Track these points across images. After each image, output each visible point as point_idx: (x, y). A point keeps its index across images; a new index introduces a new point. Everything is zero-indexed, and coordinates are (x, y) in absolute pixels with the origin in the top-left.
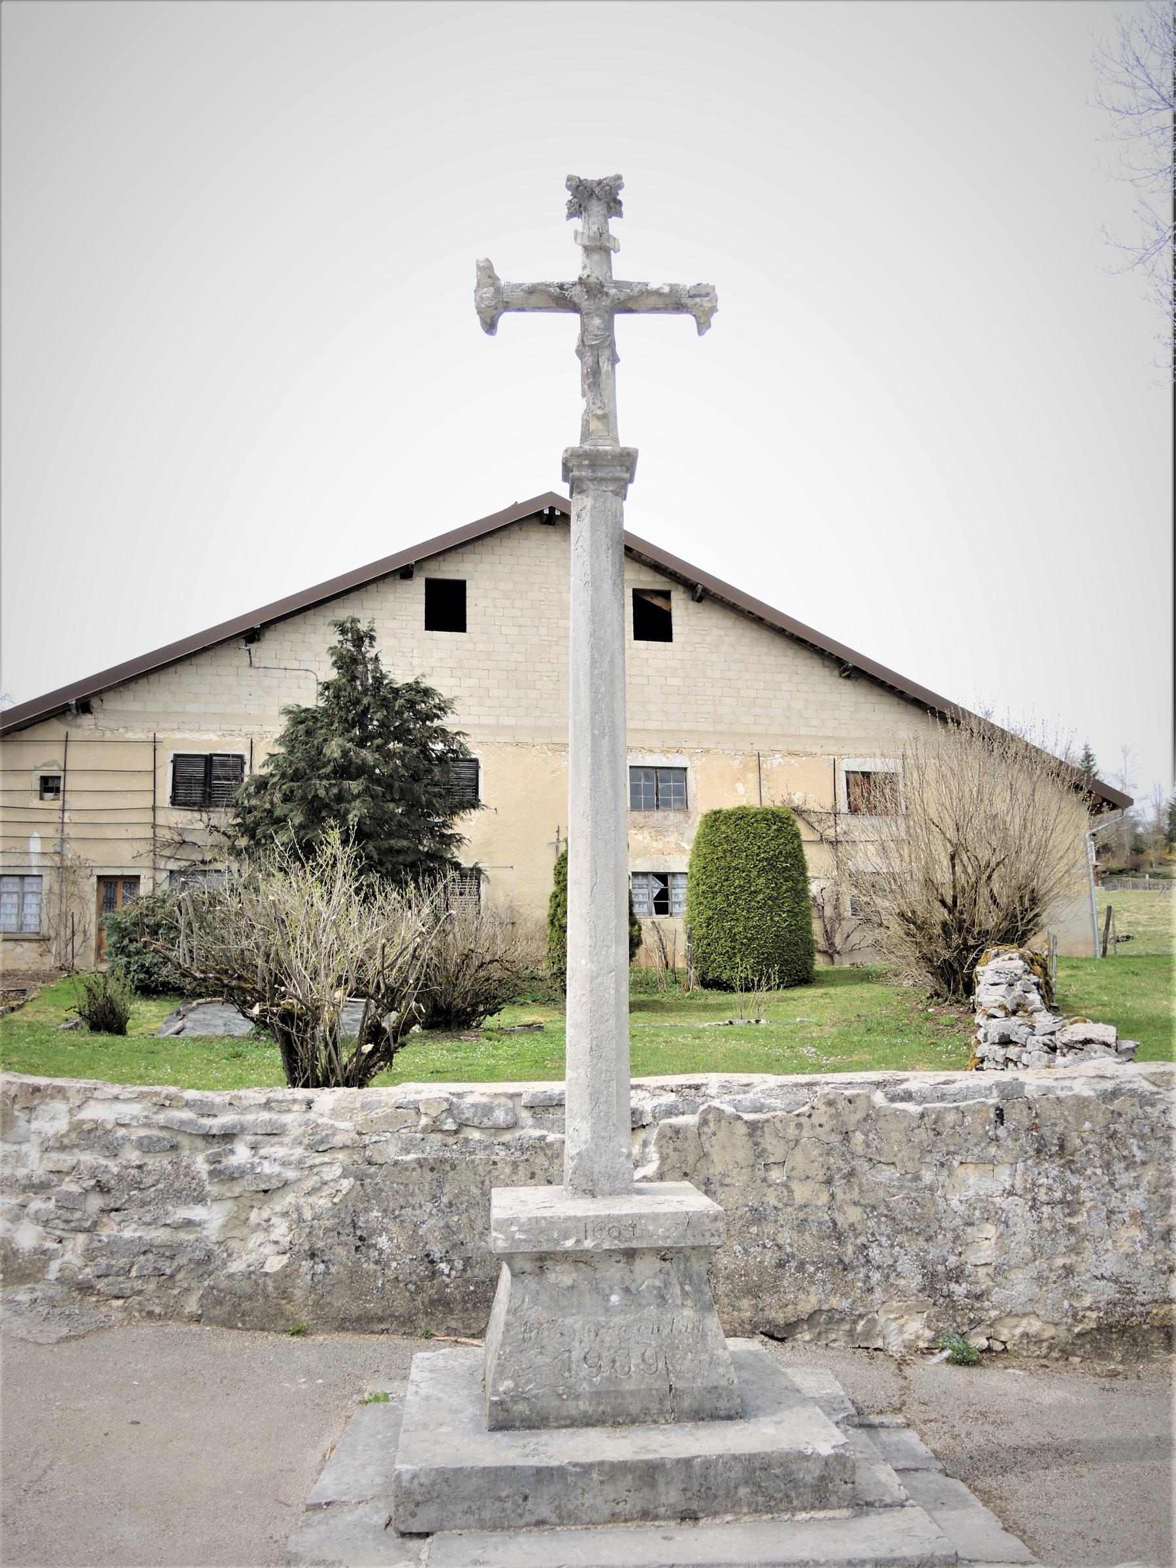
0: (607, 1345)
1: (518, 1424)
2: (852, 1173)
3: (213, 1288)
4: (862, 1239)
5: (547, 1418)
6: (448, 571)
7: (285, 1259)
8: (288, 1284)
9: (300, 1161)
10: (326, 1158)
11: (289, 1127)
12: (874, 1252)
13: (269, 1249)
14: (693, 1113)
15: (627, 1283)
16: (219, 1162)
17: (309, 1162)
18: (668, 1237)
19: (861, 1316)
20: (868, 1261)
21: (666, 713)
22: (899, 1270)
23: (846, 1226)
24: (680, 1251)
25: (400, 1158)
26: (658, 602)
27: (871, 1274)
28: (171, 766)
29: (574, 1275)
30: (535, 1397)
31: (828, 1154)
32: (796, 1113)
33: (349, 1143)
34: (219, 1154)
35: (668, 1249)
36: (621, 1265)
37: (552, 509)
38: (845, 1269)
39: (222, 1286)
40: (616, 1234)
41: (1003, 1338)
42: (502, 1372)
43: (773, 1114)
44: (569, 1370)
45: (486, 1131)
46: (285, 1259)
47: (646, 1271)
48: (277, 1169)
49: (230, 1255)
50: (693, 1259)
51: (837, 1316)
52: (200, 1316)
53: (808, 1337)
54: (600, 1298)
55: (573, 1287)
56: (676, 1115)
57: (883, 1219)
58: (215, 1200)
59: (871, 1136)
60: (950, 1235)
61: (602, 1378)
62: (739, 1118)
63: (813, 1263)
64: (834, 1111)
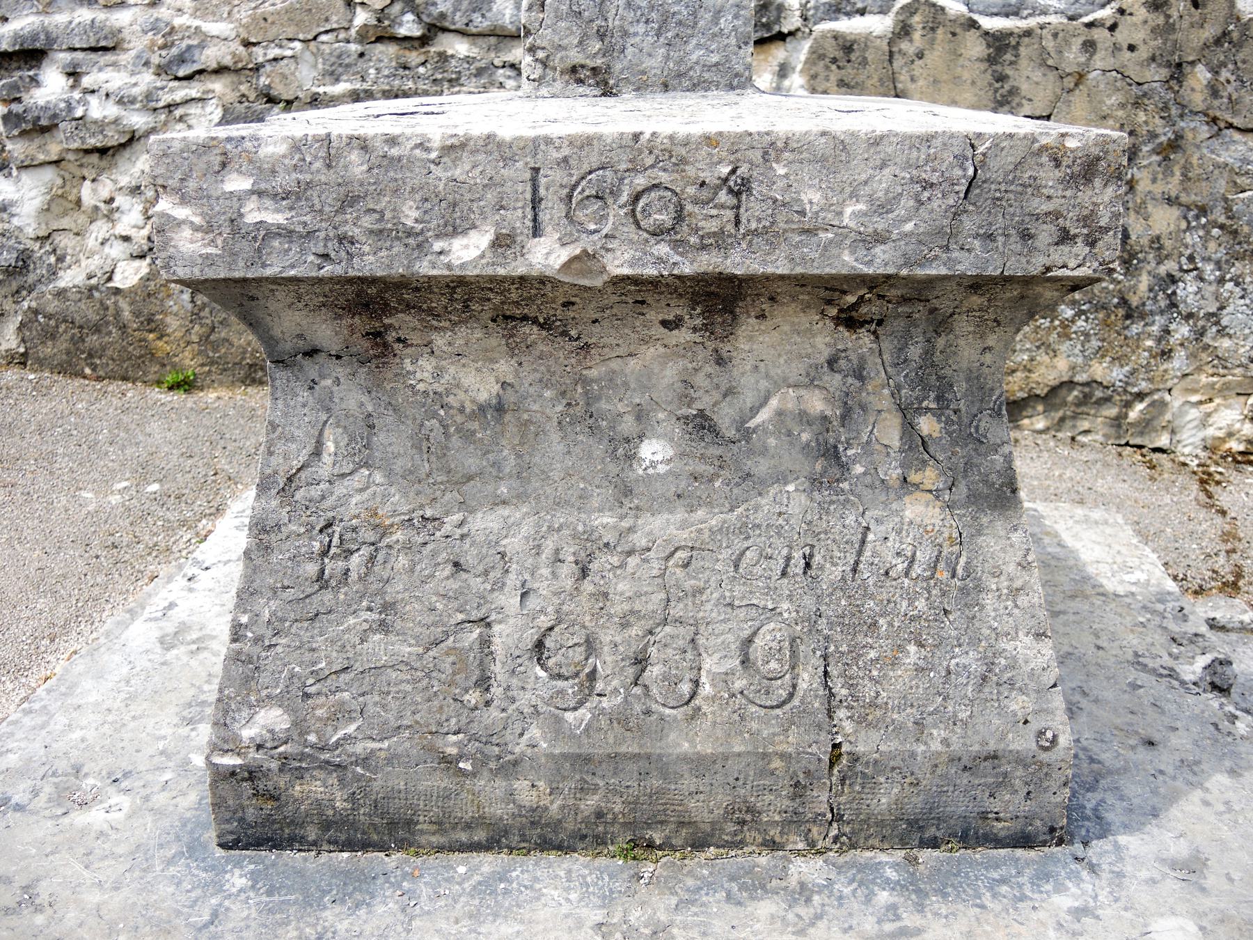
0: (618, 608)
1: (312, 833)
2: (1175, 144)
3: (36, 312)
4: (1170, 266)
5: (410, 823)
7: (143, 267)
8: (155, 309)
9: (149, 96)
10: (193, 90)
11: (126, 34)
12: (1187, 290)
13: (116, 250)
14: (883, 11)
15: (704, 402)
16: (18, 100)
17: (166, 98)
18: (880, 238)
19: (1140, 396)
20: (1173, 305)
22: (1224, 322)
23: (1145, 241)
24: (918, 292)
25: (321, 90)
27: (1172, 327)
29: (505, 367)
30: (365, 761)
31: (1136, 105)
32: (1086, 20)
33: (228, 61)
34: (15, 87)
35: (872, 283)
36: (683, 336)
38: (1128, 316)
39: (51, 309)
40: (664, 218)
42: (247, 680)
43: (1042, 19)
44: (484, 683)
45: (480, 41)
46: (143, 267)
47: (776, 367)
48: (112, 110)
49: (60, 259)
50: (963, 325)
51: (1099, 394)
52: (25, 355)
53: (1040, 425)
54: (599, 449)
55: (500, 408)
56: (848, 14)
57: (1216, 232)
58: (23, 167)
59: (1225, 74)
61: (598, 713)
62: (973, 24)
64: (1161, 20)
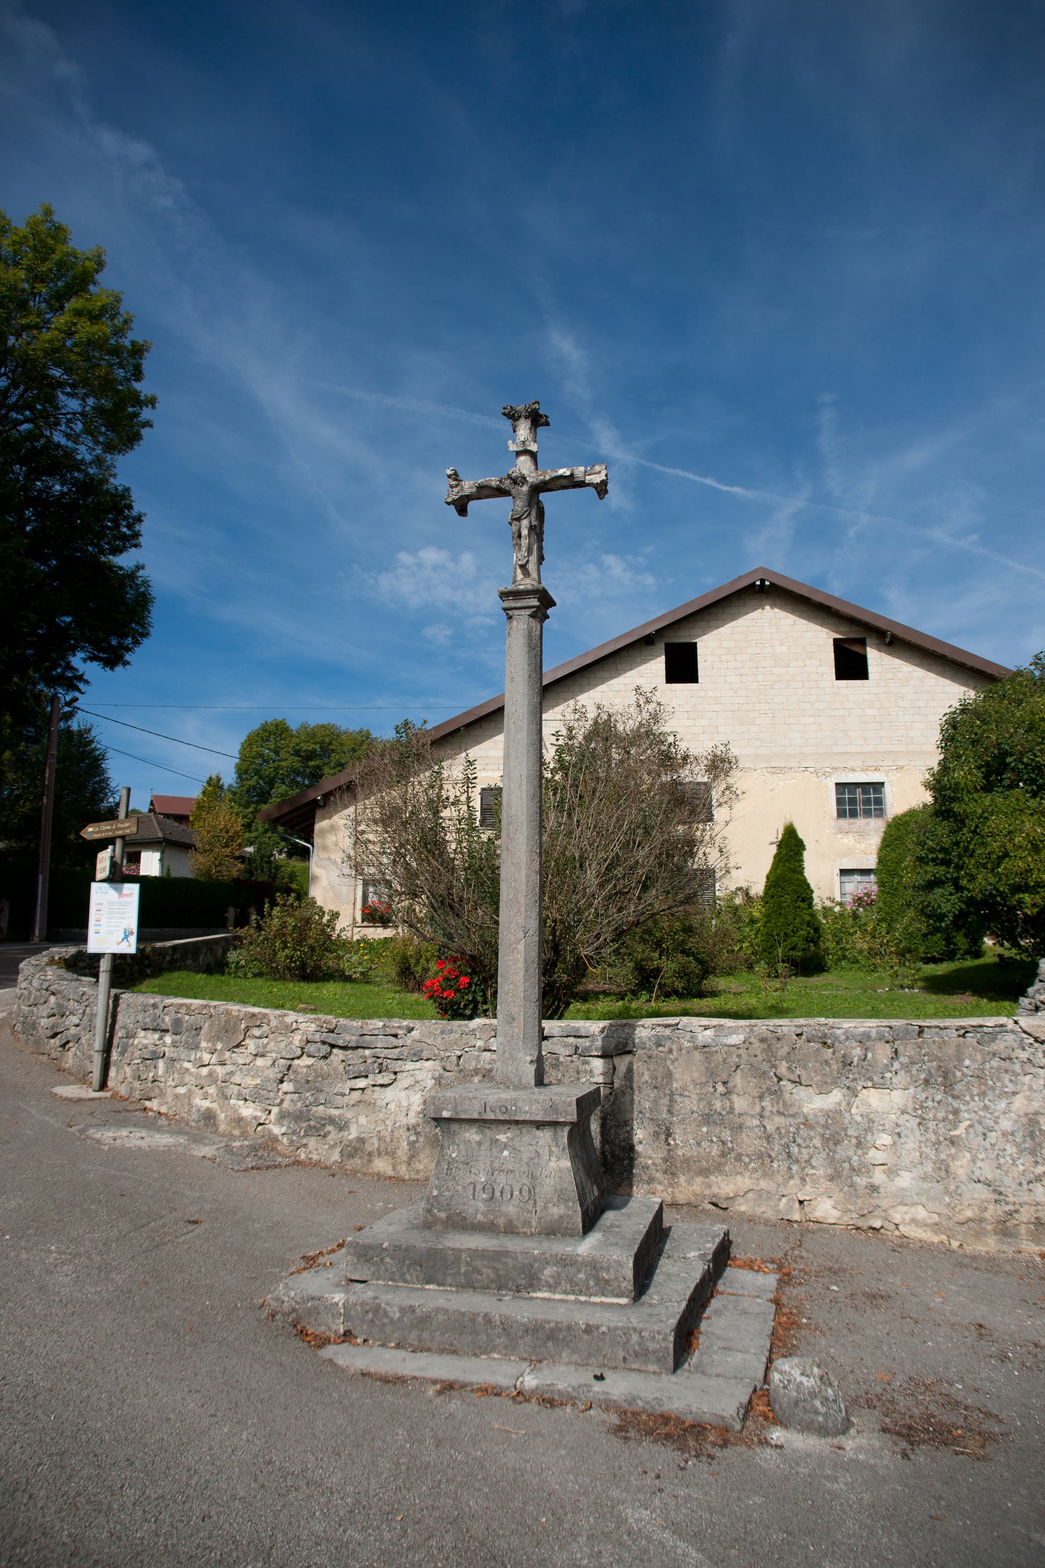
6: (682, 637)
21: (865, 738)
26: (856, 648)
28: (479, 797)
37: (763, 581)
41: (896, 1222)
60: (854, 1141)
63: (748, 1156)
